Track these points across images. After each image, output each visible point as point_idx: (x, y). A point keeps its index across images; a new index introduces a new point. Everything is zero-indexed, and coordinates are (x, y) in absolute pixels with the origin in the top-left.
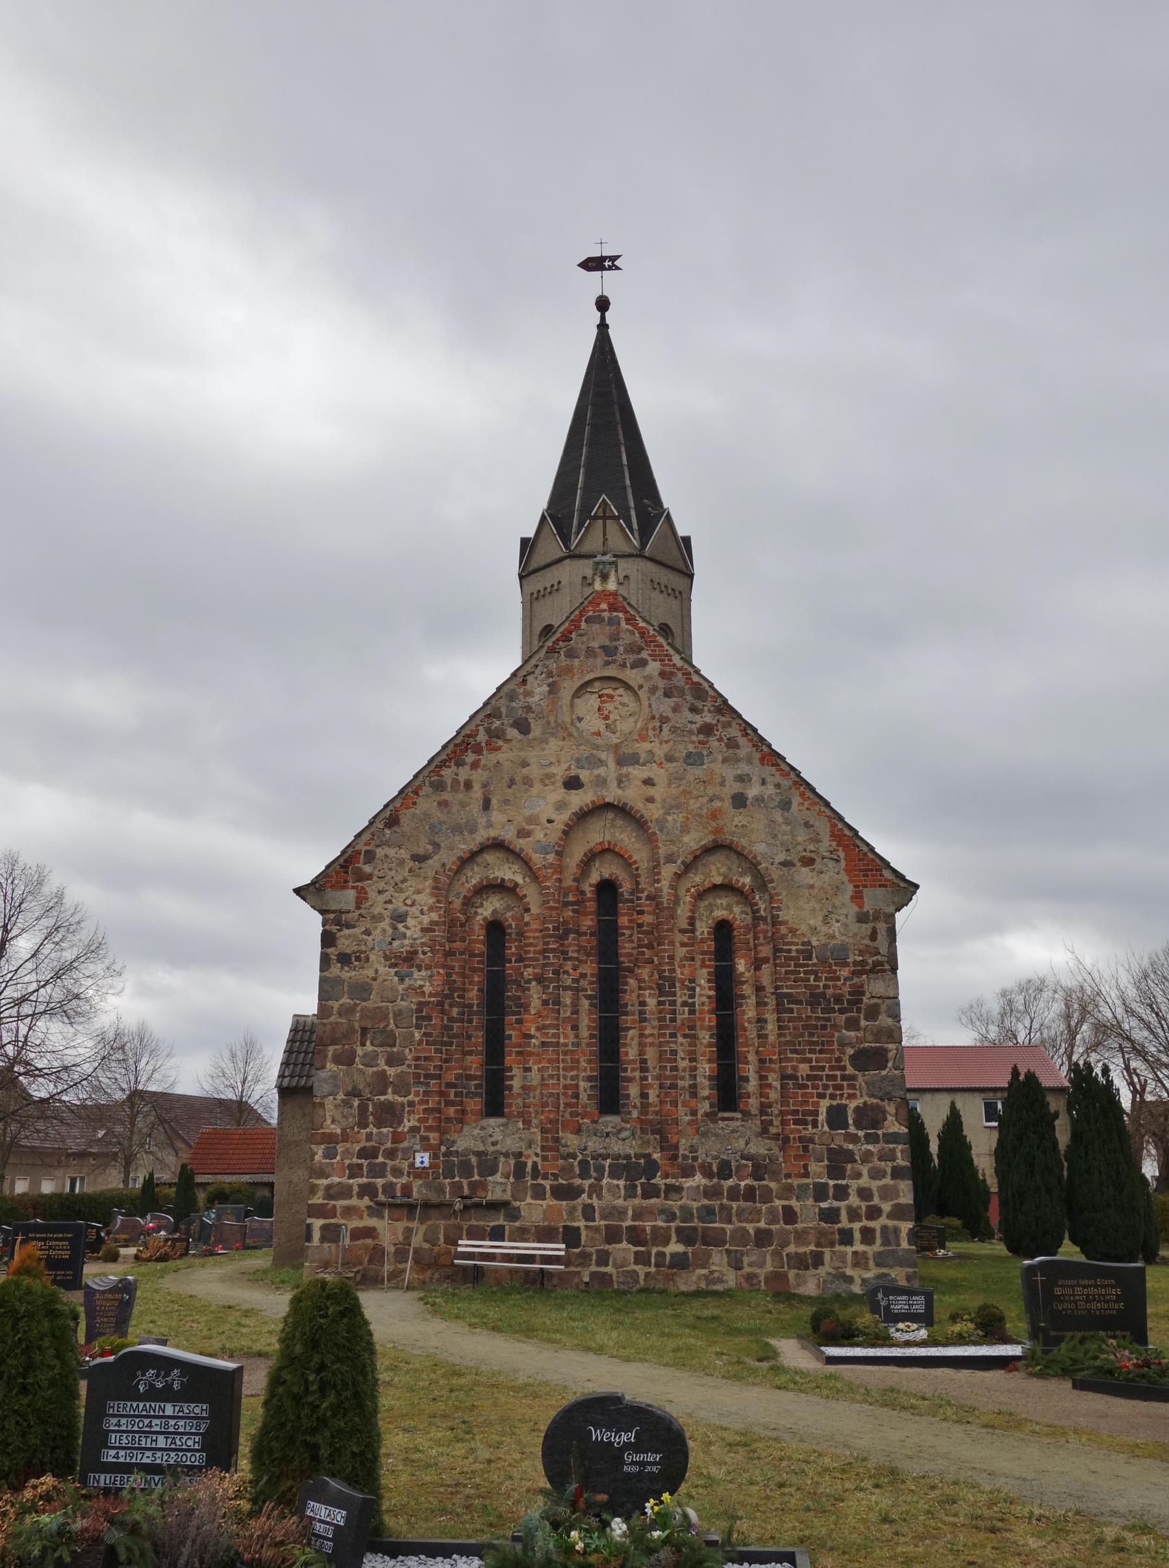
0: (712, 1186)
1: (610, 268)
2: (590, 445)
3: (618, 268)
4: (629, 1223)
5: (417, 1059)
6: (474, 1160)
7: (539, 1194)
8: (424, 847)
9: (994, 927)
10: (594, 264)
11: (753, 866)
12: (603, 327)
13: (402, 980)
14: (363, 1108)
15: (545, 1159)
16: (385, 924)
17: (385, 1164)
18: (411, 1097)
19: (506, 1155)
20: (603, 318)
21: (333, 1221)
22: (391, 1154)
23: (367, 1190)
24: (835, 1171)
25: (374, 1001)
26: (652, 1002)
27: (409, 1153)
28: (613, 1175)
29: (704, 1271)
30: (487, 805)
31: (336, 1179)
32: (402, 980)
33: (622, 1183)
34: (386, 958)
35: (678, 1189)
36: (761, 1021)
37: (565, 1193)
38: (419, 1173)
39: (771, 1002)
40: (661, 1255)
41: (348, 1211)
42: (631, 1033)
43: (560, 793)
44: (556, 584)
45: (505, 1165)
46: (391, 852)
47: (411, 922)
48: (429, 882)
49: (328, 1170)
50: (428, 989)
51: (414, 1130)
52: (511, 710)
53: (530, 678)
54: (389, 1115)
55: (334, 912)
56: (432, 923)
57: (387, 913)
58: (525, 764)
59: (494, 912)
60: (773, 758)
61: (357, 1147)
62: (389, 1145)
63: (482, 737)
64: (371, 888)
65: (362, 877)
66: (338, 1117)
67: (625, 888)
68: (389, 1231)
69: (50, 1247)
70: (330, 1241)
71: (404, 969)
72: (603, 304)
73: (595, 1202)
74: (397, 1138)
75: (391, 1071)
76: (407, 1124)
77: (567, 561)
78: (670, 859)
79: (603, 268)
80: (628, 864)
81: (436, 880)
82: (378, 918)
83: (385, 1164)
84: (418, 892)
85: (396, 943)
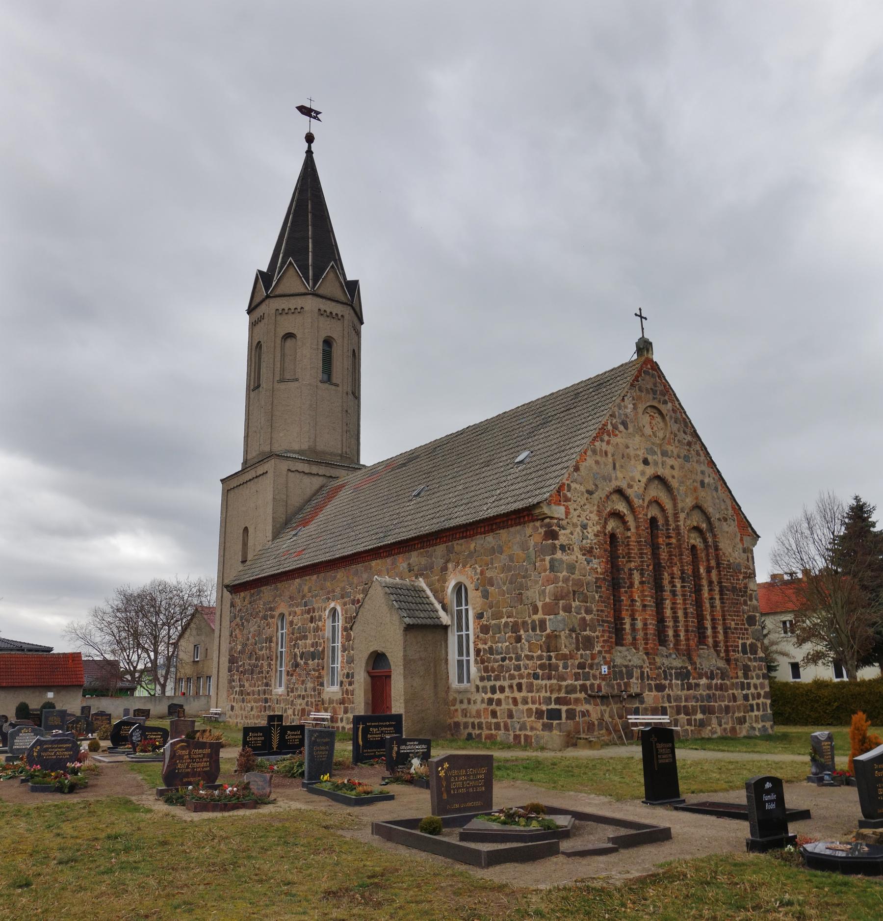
0: (836, 685)
1: (315, 118)
2: (313, 226)
3: (319, 120)
4: (683, 704)
5: (598, 611)
6: (624, 670)
7: (650, 690)
8: (591, 487)
9: (111, 530)
10: (305, 111)
11: (708, 519)
12: (309, 152)
13: (588, 563)
14: (577, 638)
15: (651, 669)
16: (578, 529)
17: (589, 672)
18: (597, 633)
19: (636, 667)
20: (310, 147)
21: (570, 707)
22: (591, 667)
23: (583, 688)
24: (746, 676)
25: (577, 576)
26: (679, 585)
27: (599, 665)
28: (677, 679)
29: (710, 728)
30: (614, 468)
31: (569, 682)
32: (588, 563)
33: (679, 682)
34: (581, 549)
35: (697, 685)
36: (712, 599)
37: (660, 688)
38: (603, 678)
39: (717, 589)
40: (695, 720)
41: (577, 700)
42: (668, 601)
43: (641, 467)
44: (299, 308)
45: (636, 673)
46: (578, 486)
47: (589, 530)
48: (595, 507)
49: (565, 676)
50: (599, 570)
51: (600, 652)
52: (620, 414)
53: (626, 398)
54: (588, 643)
55: (556, 519)
56: (598, 531)
57: (579, 523)
58: (627, 447)
59: (613, 528)
60: (712, 464)
61: (577, 662)
62: (590, 661)
63: (610, 427)
64: (572, 506)
65: (567, 500)
66: (567, 644)
67: (661, 522)
68: (595, 711)
69: (382, 732)
70: (570, 719)
71: (587, 557)
72: (310, 138)
73: (671, 693)
74: (593, 657)
75: (588, 617)
76: (597, 648)
77: (310, 296)
78: (683, 511)
79: (310, 116)
80: (663, 509)
81: (598, 506)
82: (575, 525)
83: (589, 672)
84: (591, 512)
85: (584, 541)
